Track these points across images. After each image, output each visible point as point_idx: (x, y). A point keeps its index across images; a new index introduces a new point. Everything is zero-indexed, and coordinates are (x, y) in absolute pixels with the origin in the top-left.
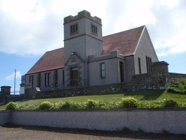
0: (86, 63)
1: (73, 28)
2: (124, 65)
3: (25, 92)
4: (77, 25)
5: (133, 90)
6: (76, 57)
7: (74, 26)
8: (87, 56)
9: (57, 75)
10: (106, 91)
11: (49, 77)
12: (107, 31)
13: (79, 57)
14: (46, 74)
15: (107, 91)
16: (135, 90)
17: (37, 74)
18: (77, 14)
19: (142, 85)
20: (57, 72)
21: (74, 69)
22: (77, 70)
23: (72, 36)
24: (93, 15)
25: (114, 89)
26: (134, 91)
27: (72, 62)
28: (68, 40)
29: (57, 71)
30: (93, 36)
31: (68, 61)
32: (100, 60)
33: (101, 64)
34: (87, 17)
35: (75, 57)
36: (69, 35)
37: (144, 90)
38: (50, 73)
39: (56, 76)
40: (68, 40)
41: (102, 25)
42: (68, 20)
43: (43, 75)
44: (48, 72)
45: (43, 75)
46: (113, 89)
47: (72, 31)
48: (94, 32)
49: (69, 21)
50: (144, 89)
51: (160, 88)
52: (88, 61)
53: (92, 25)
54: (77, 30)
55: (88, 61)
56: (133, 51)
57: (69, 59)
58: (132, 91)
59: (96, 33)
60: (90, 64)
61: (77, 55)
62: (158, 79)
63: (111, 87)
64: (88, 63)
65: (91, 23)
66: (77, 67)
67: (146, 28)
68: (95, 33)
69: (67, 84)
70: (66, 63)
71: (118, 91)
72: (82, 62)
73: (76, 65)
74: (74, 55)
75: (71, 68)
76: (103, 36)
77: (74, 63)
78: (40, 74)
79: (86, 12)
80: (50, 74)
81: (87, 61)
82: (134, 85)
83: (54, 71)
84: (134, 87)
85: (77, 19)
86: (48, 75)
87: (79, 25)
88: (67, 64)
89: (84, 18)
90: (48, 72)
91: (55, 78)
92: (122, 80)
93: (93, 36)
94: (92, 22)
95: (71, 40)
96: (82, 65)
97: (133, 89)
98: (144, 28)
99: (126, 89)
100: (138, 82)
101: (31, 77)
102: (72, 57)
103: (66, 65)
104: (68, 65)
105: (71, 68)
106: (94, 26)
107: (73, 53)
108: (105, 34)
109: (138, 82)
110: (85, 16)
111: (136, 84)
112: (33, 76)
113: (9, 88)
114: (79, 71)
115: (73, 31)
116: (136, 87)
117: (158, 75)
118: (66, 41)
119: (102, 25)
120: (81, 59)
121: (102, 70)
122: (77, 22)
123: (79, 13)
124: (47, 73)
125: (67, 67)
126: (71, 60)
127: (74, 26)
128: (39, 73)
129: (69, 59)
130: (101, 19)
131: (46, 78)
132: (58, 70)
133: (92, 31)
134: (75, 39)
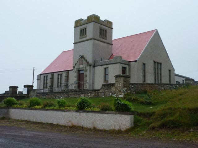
0: (92, 67)
2: (127, 69)
4: (85, 29)
5: (102, 96)
11: (61, 78)
12: (117, 34)
13: (86, 61)
17: (51, 74)
20: (68, 73)
21: (81, 72)
22: (84, 73)
23: (81, 40)
24: (102, 18)
27: (80, 65)
28: (77, 43)
31: (76, 64)
32: (104, 65)
33: (105, 68)
36: (79, 38)
39: (52, 79)
40: (77, 43)
41: (113, 28)
42: (78, 23)
43: (56, 76)
44: (61, 73)
45: (56, 76)
47: (81, 35)
49: (79, 24)
54: (85, 34)
57: (78, 61)
60: (96, 68)
61: (84, 58)
62: (119, 89)
64: (94, 66)
66: (84, 70)
69: (74, 86)
70: (75, 65)
74: (82, 59)
77: (81, 66)
78: (53, 75)
80: (107, 69)
81: (92, 65)
86: (47, 78)
90: (61, 73)
92: (170, 81)
93: (101, 39)
95: (80, 43)
96: (88, 68)
97: (103, 95)
101: (60, 75)
103: (74, 67)
105: (79, 71)
107: (81, 57)
108: (114, 38)
112: (47, 76)
113: (16, 88)
114: (85, 74)
115: (82, 34)
116: (105, 94)
117: (119, 86)
118: (75, 44)
119: (113, 28)
120: (88, 63)
122: (86, 25)
123: (88, 17)
124: (60, 74)
125: (75, 70)
128: (53, 74)
131: (58, 79)
132: (69, 71)
134: (83, 42)
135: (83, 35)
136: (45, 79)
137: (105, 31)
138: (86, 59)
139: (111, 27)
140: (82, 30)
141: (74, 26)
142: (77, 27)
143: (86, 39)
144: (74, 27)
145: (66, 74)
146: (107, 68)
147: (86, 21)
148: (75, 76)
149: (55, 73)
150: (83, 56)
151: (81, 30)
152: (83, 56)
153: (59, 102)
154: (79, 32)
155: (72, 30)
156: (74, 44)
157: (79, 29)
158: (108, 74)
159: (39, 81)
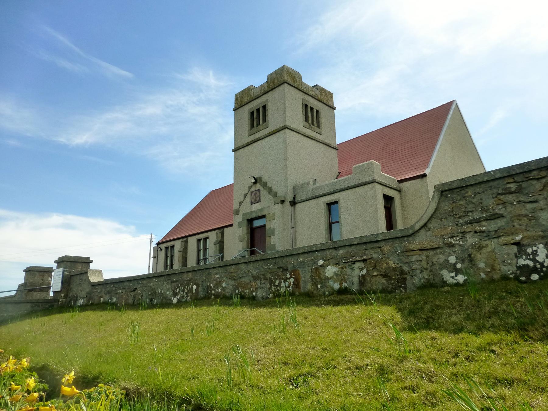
0: (287, 204)
1: (255, 116)
3: (63, 283)
4: (264, 107)
5: (448, 276)
6: (262, 189)
7: (258, 110)
8: (291, 184)
9: (223, 242)
10: (297, 284)
11: (205, 249)
13: (270, 190)
14: (199, 241)
15: (302, 285)
16: (461, 278)
18: (266, 80)
19: (517, 244)
21: (257, 223)
23: (252, 138)
25: (336, 274)
26: (457, 284)
29: (223, 231)
30: (309, 132)
33: (329, 205)
34: (290, 81)
35: (259, 191)
36: (247, 134)
37: (535, 277)
38: (208, 238)
41: (334, 108)
46: (330, 271)
47: (252, 126)
48: (313, 124)
50: (535, 270)
51: (521, 278)
52: (294, 198)
53: (306, 106)
54: (264, 121)
55: (294, 198)
56: (426, 166)
57: (245, 195)
58: (444, 283)
59: (318, 126)
60: (298, 206)
61: (265, 185)
63: (321, 262)
64: (293, 203)
65: (302, 99)
67: (457, 105)
68: (316, 125)
71: (356, 280)
72: (275, 204)
73: (261, 210)
75: (250, 221)
76: (337, 143)
77: (256, 207)
79: (287, 71)
81: (290, 198)
82: (451, 245)
83: (217, 233)
84: (452, 259)
85: (266, 93)
87: (270, 107)
88: (239, 209)
89: (282, 87)
91: (218, 248)
93: (309, 132)
94: (307, 98)
98: (453, 107)
99: (402, 273)
100: (478, 221)
102: (253, 189)
104: (241, 212)
105: (250, 221)
106: (312, 109)
109: (478, 221)
110: (286, 78)
111: (471, 240)
112: (172, 247)
114: (267, 227)
120: (275, 195)
121: (333, 221)
122: (264, 98)
126: (248, 199)
127: (258, 110)
129: (245, 195)
130: (331, 92)
131: (199, 251)
132: (225, 229)
133: (307, 120)
135: (258, 124)
136: (169, 255)
137: (317, 112)
138: (269, 185)
139: (330, 104)
140: (255, 125)
141: (233, 106)
142: (241, 109)
143: (266, 131)
144: (234, 110)
145: (217, 237)
146: (336, 202)
147: (266, 86)
148: (240, 236)
149: (191, 237)
150: (260, 178)
151: (252, 113)
152: (260, 178)
153: (114, 336)
154: (247, 119)
155: (230, 118)
156: (234, 151)
157: (246, 111)
158: (338, 222)
159: (156, 259)
